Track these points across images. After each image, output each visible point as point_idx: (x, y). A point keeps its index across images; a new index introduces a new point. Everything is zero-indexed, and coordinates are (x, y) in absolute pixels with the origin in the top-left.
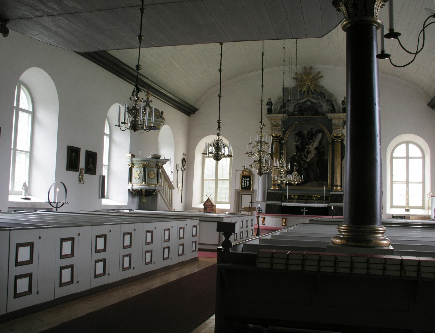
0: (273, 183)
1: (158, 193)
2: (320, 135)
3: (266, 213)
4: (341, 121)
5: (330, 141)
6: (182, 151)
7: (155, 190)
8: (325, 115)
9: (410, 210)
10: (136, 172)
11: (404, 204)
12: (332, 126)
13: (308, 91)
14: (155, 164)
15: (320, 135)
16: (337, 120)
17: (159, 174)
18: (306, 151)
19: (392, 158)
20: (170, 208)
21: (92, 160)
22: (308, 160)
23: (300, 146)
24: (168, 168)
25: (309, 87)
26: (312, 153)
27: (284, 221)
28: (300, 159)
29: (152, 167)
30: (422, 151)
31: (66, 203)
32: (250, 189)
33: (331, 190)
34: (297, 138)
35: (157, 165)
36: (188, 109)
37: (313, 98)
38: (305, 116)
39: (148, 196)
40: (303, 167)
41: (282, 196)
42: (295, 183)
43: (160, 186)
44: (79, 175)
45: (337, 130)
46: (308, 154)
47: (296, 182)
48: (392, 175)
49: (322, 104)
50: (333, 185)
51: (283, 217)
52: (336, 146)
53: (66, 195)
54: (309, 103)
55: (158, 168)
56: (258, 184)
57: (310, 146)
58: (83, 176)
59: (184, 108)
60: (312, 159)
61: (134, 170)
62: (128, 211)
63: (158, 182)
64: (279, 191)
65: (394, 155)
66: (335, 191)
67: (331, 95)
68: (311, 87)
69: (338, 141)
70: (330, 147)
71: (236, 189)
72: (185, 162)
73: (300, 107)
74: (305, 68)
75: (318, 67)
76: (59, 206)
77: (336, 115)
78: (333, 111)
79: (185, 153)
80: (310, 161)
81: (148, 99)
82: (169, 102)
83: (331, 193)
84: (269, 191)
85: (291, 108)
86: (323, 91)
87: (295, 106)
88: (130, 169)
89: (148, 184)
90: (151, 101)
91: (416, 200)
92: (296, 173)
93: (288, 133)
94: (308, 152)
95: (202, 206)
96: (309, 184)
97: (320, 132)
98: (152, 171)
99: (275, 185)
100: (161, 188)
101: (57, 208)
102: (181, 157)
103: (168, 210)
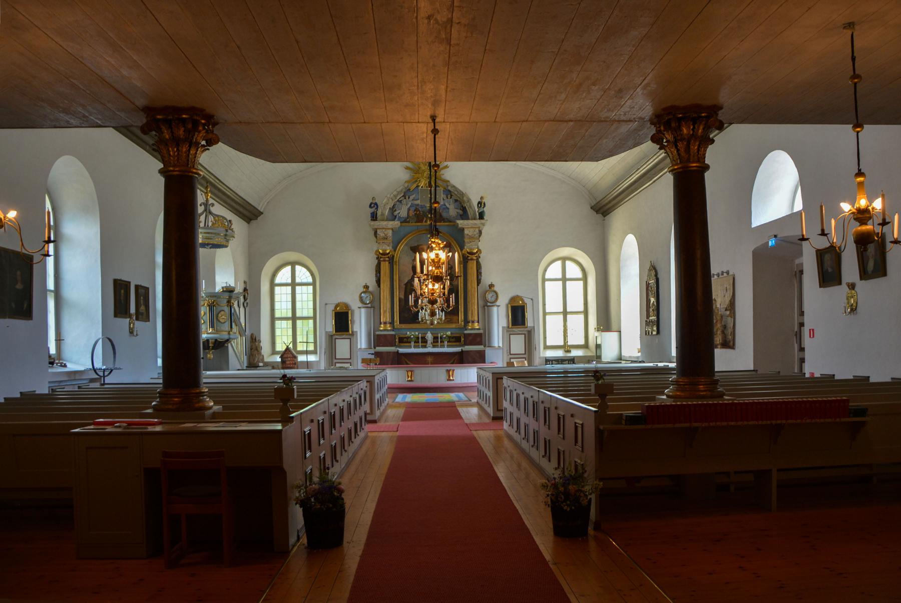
4: (477, 230)
14: (225, 301)
16: (472, 230)
19: (273, 285)
31: (116, 369)
50: (466, 321)
53: (115, 357)
56: (360, 324)
64: (393, 333)
65: (547, 277)
66: (472, 329)
69: (472, 259)
71: (326, 332)
73: (416, 210)
76: (106, 373)
77: (470, 222)
78: (464, 215)
79: (247, 280)
81: (207, 200)
83: (466, 332)
84: (377, 333)
85: (403, 212)
87: (409, 210)
89: (217, 331)
91: (575, 338)
93: (401, 247)
99: (385, 323)
101: (104, 377)
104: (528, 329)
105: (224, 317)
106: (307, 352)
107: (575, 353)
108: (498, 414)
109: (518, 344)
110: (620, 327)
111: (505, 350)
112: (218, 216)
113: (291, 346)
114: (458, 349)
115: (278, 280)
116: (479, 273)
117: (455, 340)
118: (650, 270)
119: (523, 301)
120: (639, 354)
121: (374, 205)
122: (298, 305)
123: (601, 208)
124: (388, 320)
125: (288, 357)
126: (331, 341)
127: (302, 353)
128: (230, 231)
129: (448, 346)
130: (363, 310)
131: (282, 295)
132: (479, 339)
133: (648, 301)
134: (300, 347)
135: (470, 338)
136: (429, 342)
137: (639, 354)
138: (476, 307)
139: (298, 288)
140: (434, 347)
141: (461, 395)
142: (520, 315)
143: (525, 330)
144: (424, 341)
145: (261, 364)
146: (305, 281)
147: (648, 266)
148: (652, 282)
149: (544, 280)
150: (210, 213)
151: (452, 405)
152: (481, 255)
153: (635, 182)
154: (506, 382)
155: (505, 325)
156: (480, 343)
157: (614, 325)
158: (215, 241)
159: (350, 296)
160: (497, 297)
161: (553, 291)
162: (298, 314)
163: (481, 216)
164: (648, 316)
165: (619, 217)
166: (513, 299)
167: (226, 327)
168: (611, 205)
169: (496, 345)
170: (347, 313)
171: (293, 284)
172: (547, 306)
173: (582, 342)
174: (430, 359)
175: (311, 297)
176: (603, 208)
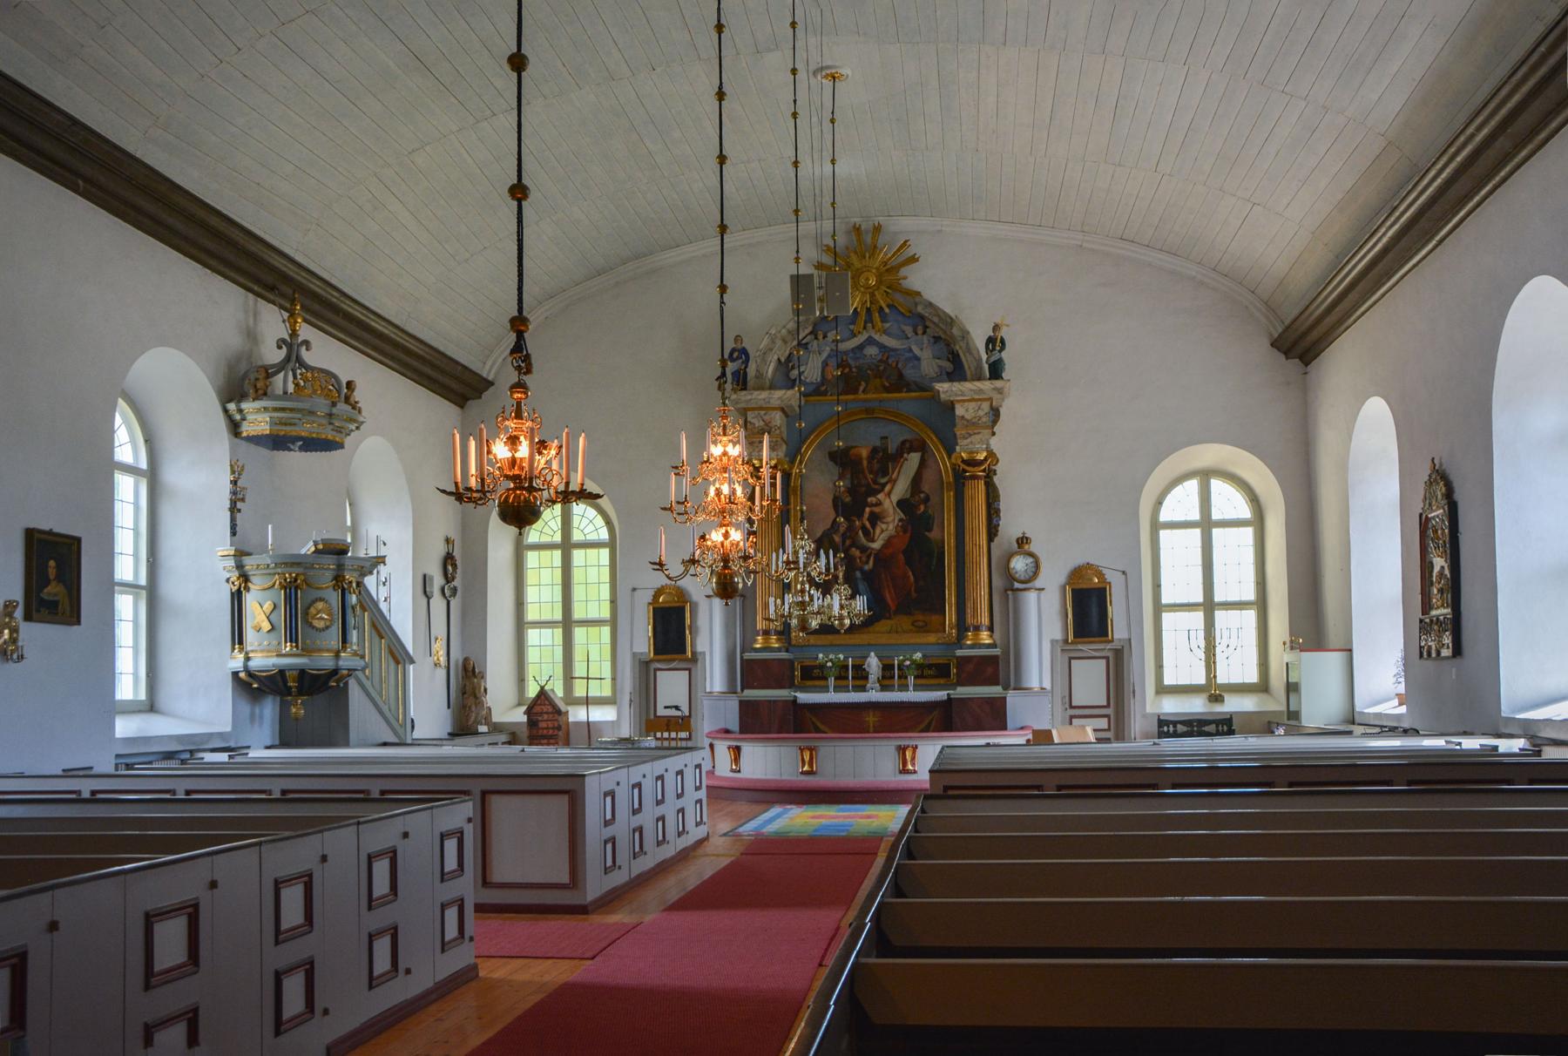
0: (761, 625)
1: (352, 683)
2: (914, 459)
3: (742, 731)
4: (986, 406)
5: (948, 477)
7: (335, 672)
8: (931, 389)
9: (1227, 697)
10: (258, 607)
11: (1201, 679)
13: (868, 310)
14: (329, 575)
15: (914, 459)
16: (973, 405)
17: (349, 611)
18: (866, 515)
20: (401, 731)
21: (58, 567)
22: (876, 545)
23: (848, 499)
24: (396, 595)
25: (872, 295)
26: (890, 519)
27: (807, 758)
28: (848, 542)
29: (323, 584)
32: (684, 652)
33: (959, 641)
34: (835, 470)
35: (338, 579)
37: (885, 332)
38: (862, 396)
39: (309, 694)
40: (861, 570)
41: (793, 669)
42: (842, 624)
43: (355, 654)
45: (973, 438)
46: (874, 526)
47: (847, 622)
49: (917, 351)
50: (962, 627)
51: (803, 744)
52: (968, 492)
54: (872, 351)
55: (343, 590)
56: (711, 631)
57: (881, 496)
60: (889, 543)
62: (224, 757)
63: (345, 641)
64: (784, 655)
67: (950, 321)
68: (878, 296)
69: (974, 477)
70: (949, 498)
72: (455, 566)
74: (857, 229)
75: (901, 226)
77: (968, 385)
78: (956, 372)
79: (452, 536)
80: (884, 546)
81: (294, 334)
82: (366, 343)
83: (959, 653)
84: (747, 656)
85: (812, 370)
86: (920, 309)
87: (825, 364)
88: (237, 598)
90: (306, 343)
91: (1239, 665)
92: (845, 590)
94: (875, 519)
95: (519, 716)
96: (884, 625)
97: (911, 450)
98: (321, 599)
99: (766, 633)
102: (440, 550)
103: (393, 739)
105: (321, 617)
106: (587, 701)
107: (1234, 704)
109: (1090, 681)
110: (1351, 641)
116: (993, 512)
117: (933, 672)
118: (1430, 483)
119: (1101, 575)
120: (1403, 709)
121: (742, 354)
122: (578, 593)
123: (1295, 343)
126: (646, 675)
128: (342, 407)
129: (917, 688)
132: (990, 670)
133: (1426, 567)
134: (579, 690)
135: (970, 667)
136: (872, 678)
137: (1403, 709)
138: (984, 592)
139: (578, 556)
140: (884, 688)
142: (1094, 610)
143: (1106, 648)
144: (861, 675)
145: (483, 729)
146: (592, 537)
147: (1424, 473)
148: (1438, 513)
149: (1156, 526)
150: (303, 364)
152: (999, 468)
153: (1386, 250)
155: (1059, 636)
156: (993, 681)
157: (681, 649)
158: (306, 429)
162: (578, 613)
163: (996, 371)
164: (1426, 606)
165: (1345, 359)
166: (1077, 573)
167: (333, 638)
168: (1315, 335)
170: (683, 609)
172: (1192, 601)
173: (1252, 676)
174: (871, 719)
175: (606, 572)
176: (1301, 342)
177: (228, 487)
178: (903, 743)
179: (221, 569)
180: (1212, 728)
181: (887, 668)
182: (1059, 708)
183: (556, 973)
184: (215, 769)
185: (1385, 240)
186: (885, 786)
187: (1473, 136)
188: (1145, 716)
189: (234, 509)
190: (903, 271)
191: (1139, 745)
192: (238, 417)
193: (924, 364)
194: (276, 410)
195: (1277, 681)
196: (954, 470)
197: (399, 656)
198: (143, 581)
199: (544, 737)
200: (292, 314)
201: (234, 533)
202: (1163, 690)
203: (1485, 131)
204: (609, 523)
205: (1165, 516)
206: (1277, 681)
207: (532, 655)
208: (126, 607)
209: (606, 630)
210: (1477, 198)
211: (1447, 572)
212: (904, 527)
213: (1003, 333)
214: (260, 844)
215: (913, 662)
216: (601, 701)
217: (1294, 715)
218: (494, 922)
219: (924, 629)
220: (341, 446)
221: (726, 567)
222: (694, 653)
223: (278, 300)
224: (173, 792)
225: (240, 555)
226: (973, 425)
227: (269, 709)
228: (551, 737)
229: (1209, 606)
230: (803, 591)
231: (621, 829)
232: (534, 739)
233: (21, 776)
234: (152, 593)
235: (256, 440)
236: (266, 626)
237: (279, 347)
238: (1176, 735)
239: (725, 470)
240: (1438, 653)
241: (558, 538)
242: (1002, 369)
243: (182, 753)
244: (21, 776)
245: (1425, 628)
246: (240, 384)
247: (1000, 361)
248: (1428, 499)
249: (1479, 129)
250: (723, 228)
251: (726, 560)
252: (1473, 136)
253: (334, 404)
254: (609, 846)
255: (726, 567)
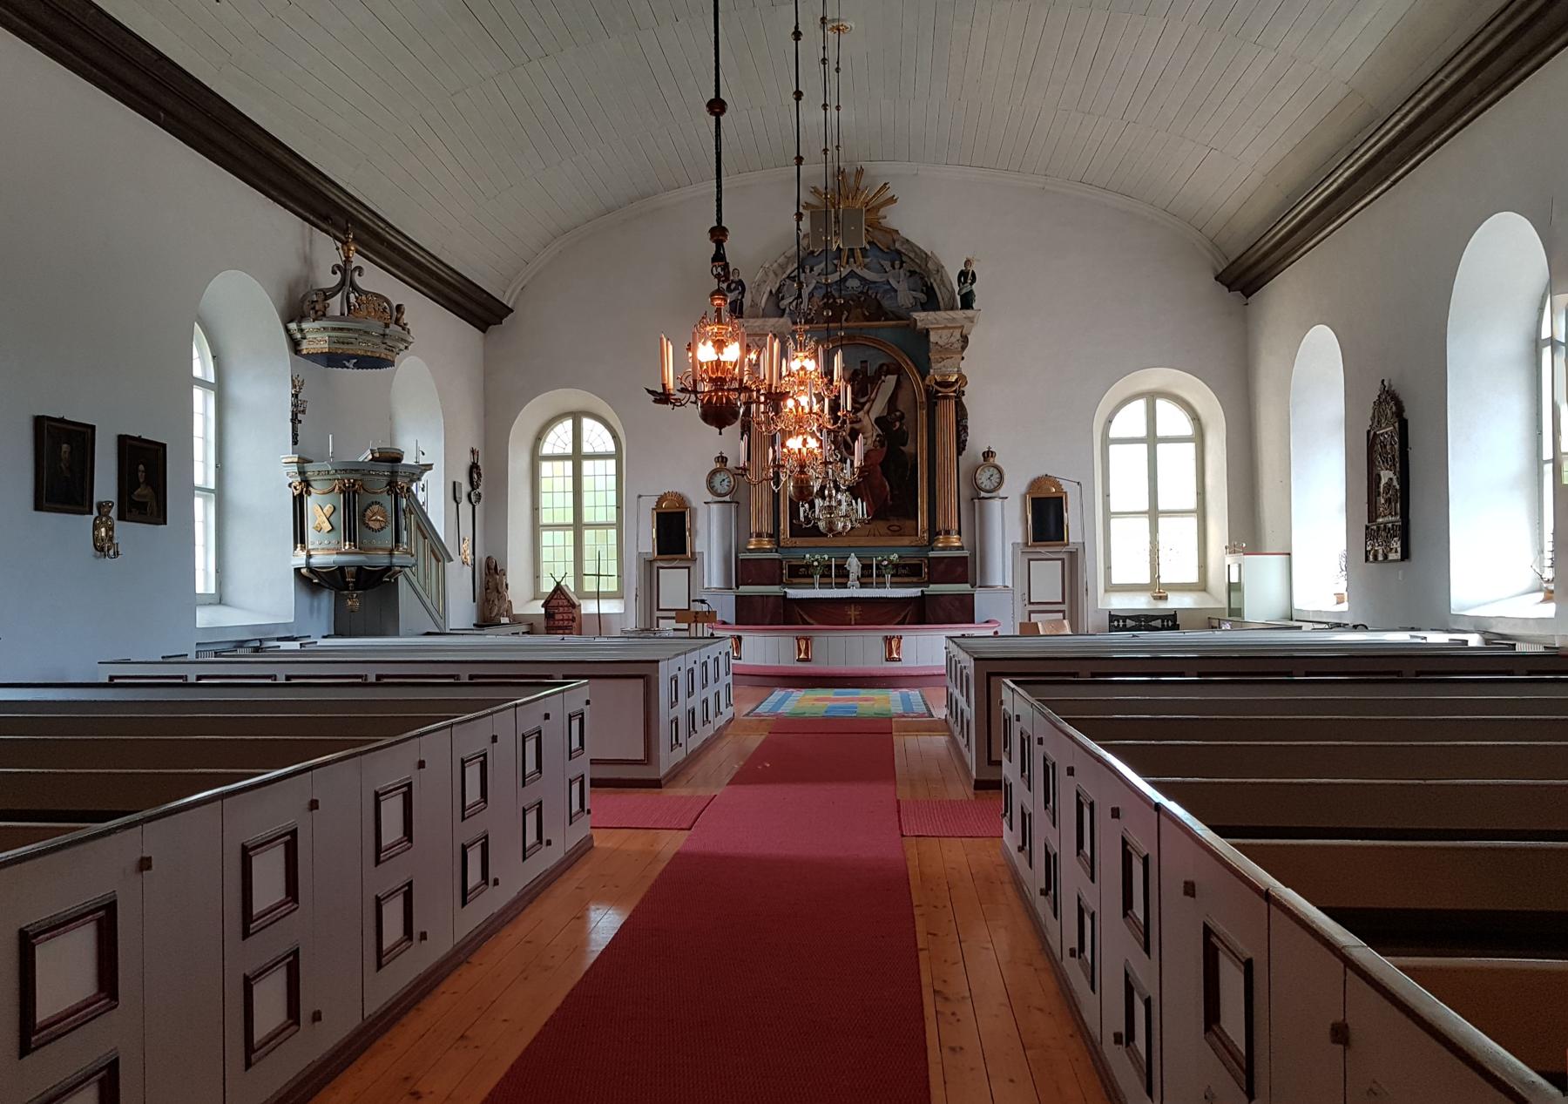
1: (401, 578)
3: (740, 621)
4: (957, 334)
6: (469, 438)
7: (389, 568)
10: (319, 510)
11: (1145, 578)
12: (928, 350)
14: (384, 481)
16: (946, 333)
19: (536, 459)
21: (146, 471)
24: (432, 496)
29: (373, 490)
30: (1196, 419)
32: (684, 552)
33: (930, 545)
36: (479, 309)
37: (865, 266)
44: (96, 527)
48: (1106, 495)
50: (933, 532)
54: (853, 283)
56: (710, 536)
58: (110, 529)
59: (468, 305)
61: (312, 504)
64: (776, 556)
65: (1113, 434)
67: (927, 258)
69: (946, 397)
70: (922, 415)
72: (479, 475)
75: (880, 171)
77: (942, 314)
81: (348, 260)
82: (404, 271)
83: (931, 554)
84: (741, 556)
86: (897, 245)
88: (299, 502)
90: (359, 269)
95: (538, 608)
97: (888, 373)
99: (759, 535)
100: (410, 560)
102: (467, 460)
104: (1071, 548)
105: (376, 518)
106: (598, 596)
107: (1176, 602)
108: (989, 775)
109: (1047, 579)
111: (1018, 597)
112: (366, 293)
113: (569, 583)
114: (914, 592)
115: (546, 449)
116: (961, 429)
117: (908, 571)
118: (1379, 403)
119: (1058, 486)
120: (1344, 607)
122: (587, 499)
123: (1238, 278)
124: (767, 527)
125: (560, 611)
126: (650, 572)
127: (589, 596)
129: (894, 585)
130: (714, 507)
131: (556, 476)
132: (960, 570)
134: (589, 585)
135: (942, 567)
137: (1549, 610)
138: (954, 501)
139: (587, 466)
140: (863, 585)
141: (914, 694)
144: (843, 573)
146: (600, 449)
148: (1387, 430)
149: (1107, 441)
150: (355, 288)
151: (880, 730)
154: (1014, 700)
155: (1020, 540)
157: (1271, 537)
158: (360, 348)
159: (688, 479)
160: (1001, 478)
161: (1127, 466)
162: (588, 517)
163: (967, 301)
164: (1373, 514)
165: (1285, 292)
166: (1037, 483)
169: (998, 582)
170: (683, 514)
171: (577, 457)
173: (1193, 577)
174: (853, 612)
175: (612, 481)
176: (1245, 276)
177: (289, 399)
178: (889, 634)
179: (284, 475)
180: (1158, 623)
181: (866, 568)
182: (1019, 605)
183: (671, 843)
184: (290, 659)
185: (1340, 180)
186: (860, 673)
187: (1442, 82)
188: (1097, 611)
189: (295, 420)
190: (882, 212)
191: (1098, 639)
192: (299, 336)
193: (900, 295)
194: (334, 329)
195: (1217, 582)
196: (927, 391)
197: (439, 554)
198: (212, 486)
199: (560, 628)
200: (344, 243)
201: (295, 442)
202: (1111, 588)
203: (1455, 77)
204: (615, 437)
205: (1114, 432)
206: (1217, 582)
207: (546, 554)
208: (203, 512)
209: (613, 532)
210: (1436, 142)
211: (1395, 483)
212: (881, 441)
213: (974, 268)
214: (451, 725)
215: (890, 562)
216: (609, 596)
217: (1236, 613)
218: (610, 798)
219: (899, 533)
220: (391, 364)
221: (802, 472)
222: (693, 553)
223: (332, 230)
224: (274, 677)
225: (302, 462)
226: (946, 350)
227: (326, 600)
228: (566, 628)
229: (1154, 513)
230: (830, 496)
231: (680, 711)
232: (550, 630)
233: (127, 662)
234: (220, 494)
235: (313, 357)
236: (327, 527)
237: (334, 273)
238: (1125, 629)
239: (802, 383)
240: (1386, 557)
241: (569, 450)
242: (972, 300)
243: (256, 644)
244: (127, 662)
245: (1371, 534)
246: (300, 307)
247: (971, 292)
248: (1377, 418)
249: (1447, 77)
250: (799, 160)
251: (802, 466)
252: (1442, 82)
253: (387, 326)
254: (575, 724)
255: (802, 472)
